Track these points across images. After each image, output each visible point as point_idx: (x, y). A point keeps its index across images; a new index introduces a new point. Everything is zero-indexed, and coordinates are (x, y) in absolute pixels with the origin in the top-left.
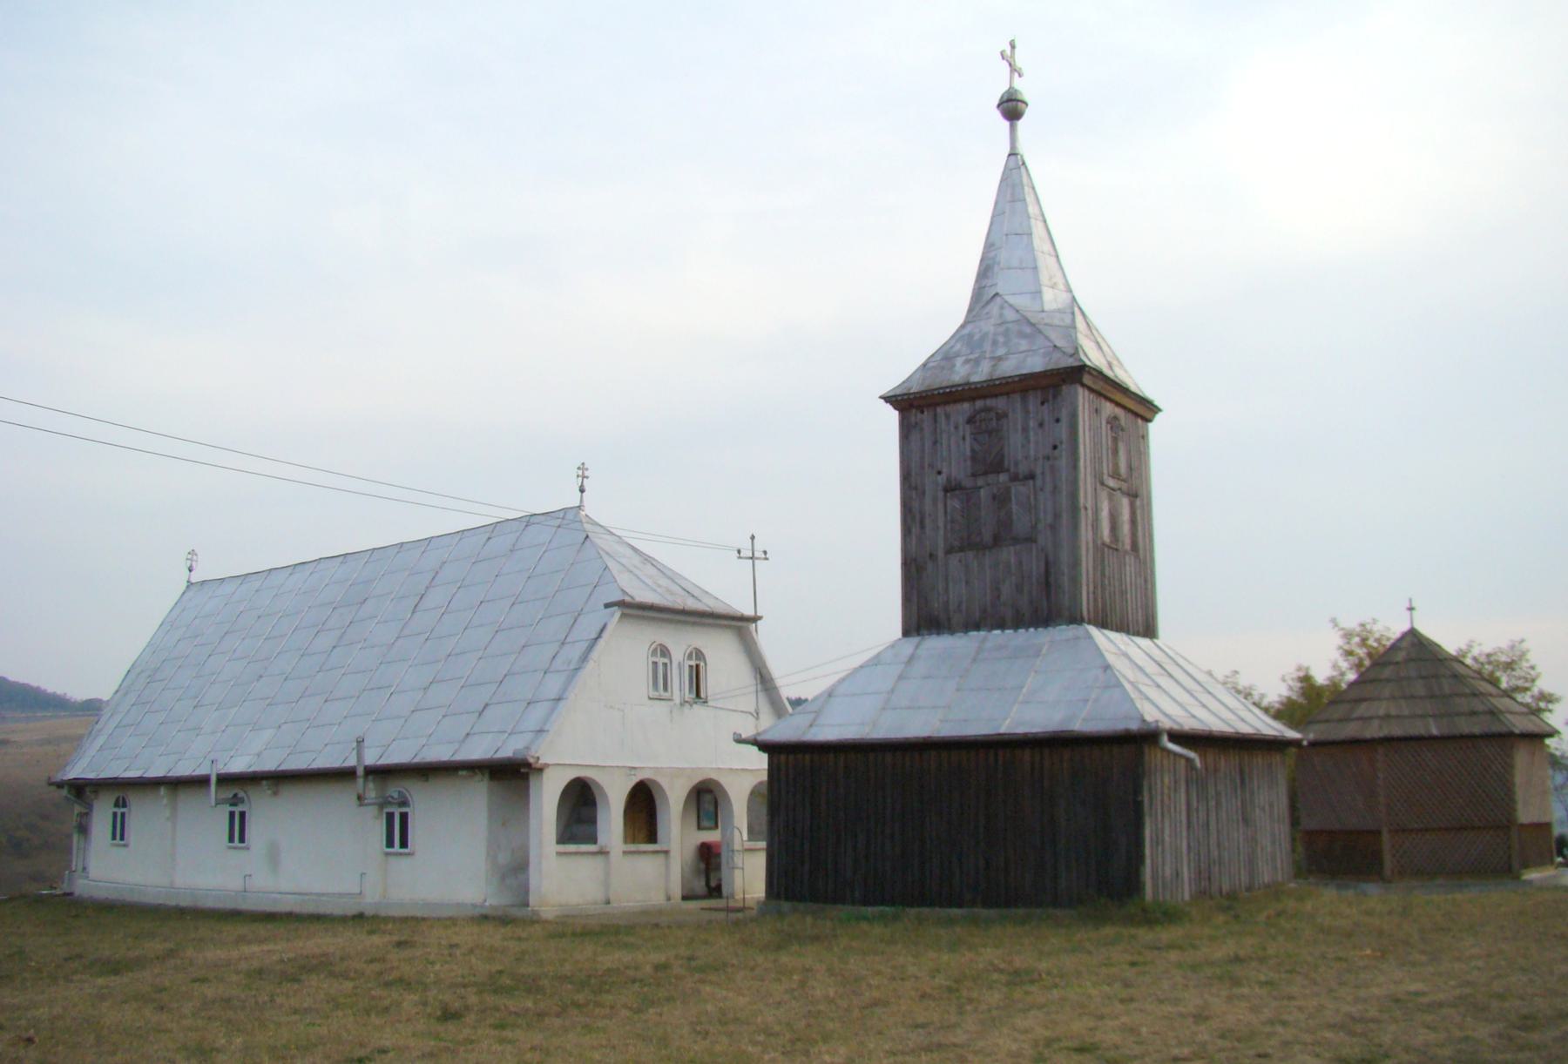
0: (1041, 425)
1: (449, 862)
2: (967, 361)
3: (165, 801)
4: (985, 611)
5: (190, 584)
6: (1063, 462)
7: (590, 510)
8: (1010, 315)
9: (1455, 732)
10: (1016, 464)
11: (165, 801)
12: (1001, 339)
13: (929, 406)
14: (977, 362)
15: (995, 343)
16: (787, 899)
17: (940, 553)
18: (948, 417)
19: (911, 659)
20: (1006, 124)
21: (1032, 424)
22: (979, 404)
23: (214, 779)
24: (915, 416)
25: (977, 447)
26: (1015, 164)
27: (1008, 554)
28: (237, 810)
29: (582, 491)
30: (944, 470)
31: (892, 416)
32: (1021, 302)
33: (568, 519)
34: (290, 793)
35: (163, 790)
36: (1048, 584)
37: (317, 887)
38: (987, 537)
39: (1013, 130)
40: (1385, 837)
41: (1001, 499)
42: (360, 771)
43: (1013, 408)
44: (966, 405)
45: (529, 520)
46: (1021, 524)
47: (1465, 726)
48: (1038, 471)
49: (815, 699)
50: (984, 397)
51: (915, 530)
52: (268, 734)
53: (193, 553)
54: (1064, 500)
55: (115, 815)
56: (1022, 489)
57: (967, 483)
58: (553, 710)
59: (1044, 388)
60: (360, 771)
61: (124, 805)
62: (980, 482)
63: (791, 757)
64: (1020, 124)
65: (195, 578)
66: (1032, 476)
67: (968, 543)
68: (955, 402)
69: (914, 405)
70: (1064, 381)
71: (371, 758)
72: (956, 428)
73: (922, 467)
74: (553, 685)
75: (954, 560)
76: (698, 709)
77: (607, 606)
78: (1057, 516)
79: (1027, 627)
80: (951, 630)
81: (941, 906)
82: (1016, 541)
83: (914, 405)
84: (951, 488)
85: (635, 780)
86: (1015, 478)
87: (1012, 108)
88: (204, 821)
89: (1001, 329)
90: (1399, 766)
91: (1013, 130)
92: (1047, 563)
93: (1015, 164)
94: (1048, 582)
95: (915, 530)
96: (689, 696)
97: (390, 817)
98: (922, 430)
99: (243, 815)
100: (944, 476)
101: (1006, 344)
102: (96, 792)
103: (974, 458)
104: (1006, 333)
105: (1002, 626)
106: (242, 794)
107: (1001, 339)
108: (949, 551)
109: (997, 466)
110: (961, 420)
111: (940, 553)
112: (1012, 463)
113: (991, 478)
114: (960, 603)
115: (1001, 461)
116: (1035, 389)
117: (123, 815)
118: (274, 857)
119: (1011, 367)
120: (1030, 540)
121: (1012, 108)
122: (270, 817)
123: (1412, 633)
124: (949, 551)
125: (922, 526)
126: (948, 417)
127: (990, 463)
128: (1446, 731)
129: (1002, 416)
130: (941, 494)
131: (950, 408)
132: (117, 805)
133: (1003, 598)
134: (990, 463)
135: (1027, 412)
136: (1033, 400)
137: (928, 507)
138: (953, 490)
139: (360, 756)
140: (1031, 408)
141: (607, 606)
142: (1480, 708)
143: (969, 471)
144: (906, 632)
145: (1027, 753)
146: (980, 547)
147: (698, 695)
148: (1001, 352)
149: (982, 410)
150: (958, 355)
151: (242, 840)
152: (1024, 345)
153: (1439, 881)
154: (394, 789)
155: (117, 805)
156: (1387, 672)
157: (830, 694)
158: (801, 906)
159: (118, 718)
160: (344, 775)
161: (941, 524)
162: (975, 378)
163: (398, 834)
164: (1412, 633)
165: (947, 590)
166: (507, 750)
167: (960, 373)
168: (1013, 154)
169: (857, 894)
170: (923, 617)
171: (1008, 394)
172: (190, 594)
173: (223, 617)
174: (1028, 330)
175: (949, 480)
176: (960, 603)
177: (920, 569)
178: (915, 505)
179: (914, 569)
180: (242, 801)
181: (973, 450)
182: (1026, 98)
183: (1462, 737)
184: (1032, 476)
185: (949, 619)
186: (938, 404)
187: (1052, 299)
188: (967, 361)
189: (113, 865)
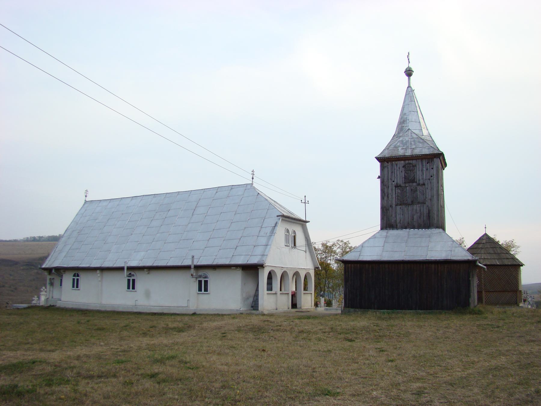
0: (427, 169)
1: (226, 296)
2: (402, 149)
3: (99, 275)
5: (86, 202)
6: (435, 181)
7: (254, 185)
8: (415, 136)
9: (492, 263)
10: (419, 180)
11: (99, 275)
12: (413, 143)
14: (406, 149)
15: (411, 144)
16: (351, 308)
17: (394, 206)
18: (397, 165)
19: (386, 237)
21: (424, 169)
22: (407, 162)
23: (126, 268)
24: (386, 164)
25: (406, 175)
27: (416, 207)
28: (131, 279)
29: (253, 179)
30: (395, 181)
31: (378, 164)
32: (417, 132)
33: (249, 187)
34: (154, 274)
35: (98, 272)
36: (429, 216)
37: (167, 304)
38: (409, 201)
39: (409, 80)
40: (483, 292)
41: (414, 191)
42: (192, 267)
43: (419, 164)
44: (403, 162)
45: (232, 187)
46: (421, 198)
47: (506, 262)
49: (359, 246)
50: (409, 160)
51: (386, 198)
52: (142, 254)
53: (87, 191)
54: (435, 192)
55: (74, 279)
56: (421, 188)
57: (403, 185)
58: (266, 248)
60: (192, 267)
61: (78, 276)
62: (407, 185)
63: (353, 265)
64: (411, 77)
65: (88, 199)
66: (424, 184)
67: (402, 203)
68: (399, 160)
69: (384, 161)
70: (435, 157)
71: (196, 263)
72: (399, 168)
74: (263, 241)
75: (398, 207)
76: (294, 250)
77: (277, 216)
78: (432, 196)
79: (422, 228)
82: (419, 203)
84: (397, 186)
85: (283, 271)
86: (419, 185)
87: (409, 73)
88: (122, 279)
89: (413, 140)
90: (489, 272)
91: (409, 80)
93: (410, 92)
94: (429, 215)
95: (386, 198)
96: (293, 245)
97: (200, 282)
98: (388, 168)
99: (134, 280)
100: (395, 182)
101: (415, 144)
102: (64, 271)
103: (405, 177)
104: (414, 141)
105: (414, 228)
106: (133, 273)
107: (413, 143)
109: (413, 181)
110: (401, 166)
111: (394, 206)
112: (411, 180)
114: (400, 220)
115: (414, 179)
116: (425, 159)
117: (78, 280)
118: (148, 294)
119: (417, 152)
120: (424, 203)
121: (409, 73)
122: (143, 281)
123: (486, 234)
125: (388, 197)
126: (397, 165)
127: (410, 179)
128: (501, 264)
129: (414, 166)
130: (394, 188)
132: (74, 276)
133: (415, 220)
134: (410, 179)
135: (423, 165)
136: (424, 162)
137: (390, 191)
139: (193, 261)
140: (424, 164)
141: (277, 216)
142: (509, 257)
144: (382, 229)
145: (367, 265)
146: (407, 204)
147: (295, 245)
148: (414, 147)
150: (399, 147)
151: (77, 287)
152: (421, 145)
153: (498, 306)
154: (201, 272)
155: (74, 276)
156: (480, 246)
157: (362, 246)
158: (357, 310)
159: (68, 247)
160: (188, 267)
161: (394, 196)
162: (406, 154)
163: (203, 286)
164: (486, 234)
165: (396, 216)
166: (254, 260)
167: (401, 152)
168: (409, 87)
170: (388, 223)
172: (86, 205)
173: (97, 214)
174: (421, 141)
175: (397, 184)
176: (400, 220)
177: (387, 210)
178: (386, 190)
179: (385, 210)
180: (133, 275)
182: (413, 70)
183: (506, 265)
184: (424, 184)
185: (397, 225)
187: (425, 132)
188: (402, 149)
189: (67, 295)
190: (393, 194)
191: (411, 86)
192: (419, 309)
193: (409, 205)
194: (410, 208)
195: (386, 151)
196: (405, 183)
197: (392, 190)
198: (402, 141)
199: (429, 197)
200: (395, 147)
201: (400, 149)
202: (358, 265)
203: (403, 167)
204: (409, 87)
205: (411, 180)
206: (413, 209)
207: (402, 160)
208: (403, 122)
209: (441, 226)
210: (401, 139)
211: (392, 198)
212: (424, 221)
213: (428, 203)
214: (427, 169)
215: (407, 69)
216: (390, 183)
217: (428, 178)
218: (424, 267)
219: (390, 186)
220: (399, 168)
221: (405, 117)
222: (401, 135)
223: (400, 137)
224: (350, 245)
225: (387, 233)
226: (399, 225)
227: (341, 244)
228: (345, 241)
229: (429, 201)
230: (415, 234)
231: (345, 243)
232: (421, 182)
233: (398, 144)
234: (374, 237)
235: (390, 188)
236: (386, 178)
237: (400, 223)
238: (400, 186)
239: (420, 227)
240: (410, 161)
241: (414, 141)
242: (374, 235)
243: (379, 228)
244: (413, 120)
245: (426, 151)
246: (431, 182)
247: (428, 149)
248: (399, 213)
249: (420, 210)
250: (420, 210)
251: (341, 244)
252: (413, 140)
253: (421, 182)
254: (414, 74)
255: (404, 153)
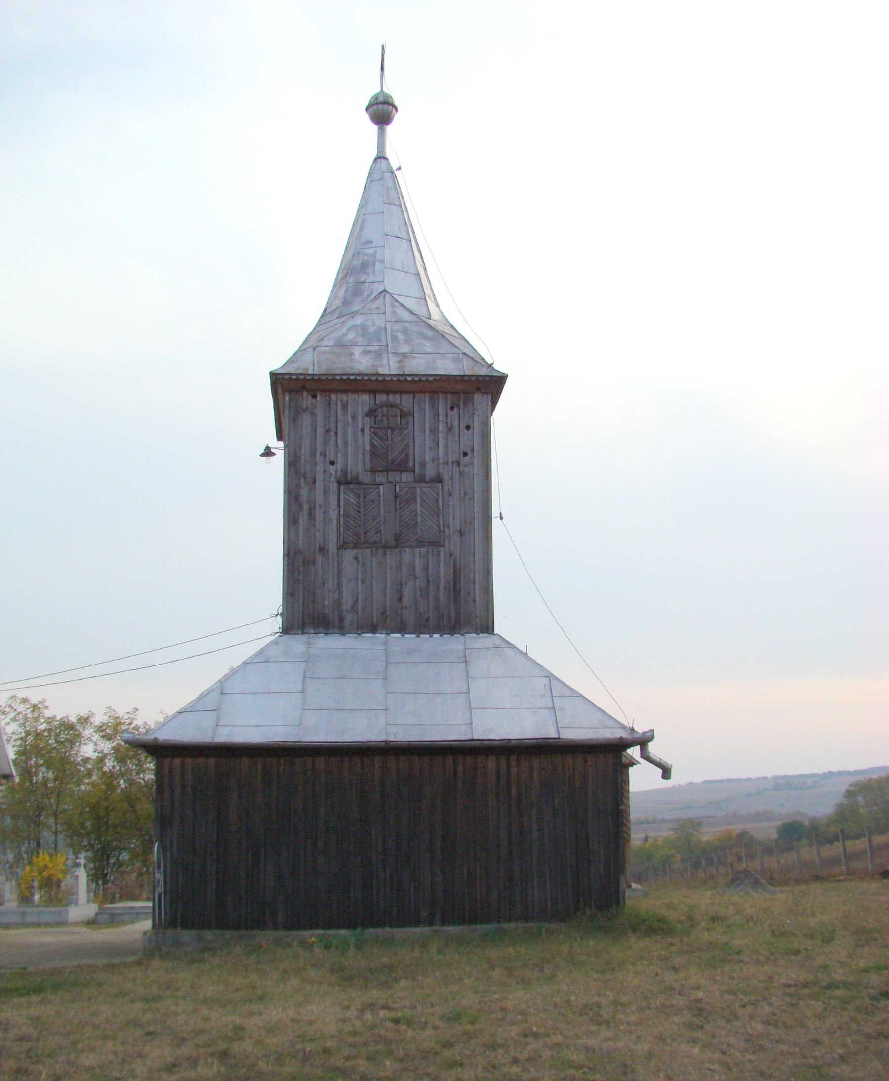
4: (384, 613)
8: (406, 316)
10: (423, 465)
12: (401, 337)
13: (323, 391)
14: (378, 355)
15: (394, 339)
16: (185, 926)
17: (332, 548)
18: (345, 406)
19: (307, 659)
20: (375, 128)
22: (382, 398)
26: (382, 177)
36: (456, 591)
38: (388, 535)
41: (401, 500)
43: (423, 411)
44: (366, 397)
48: (446, 477)
50: (388, 392)
51: (303, 520)
56: (427, 490)
57: (365, 478)
59: (455, 393)
62: (380, 478)
64: (390, 129)
67: (357, 539)
70: (478, 389)
72: (354, 418)
73: (313, 455)
75: (348, 555)
79: (431, 632)
80: (342, 630)
81: (391, 926)
82: (421, 543)
83: (289, 388)
84: (345, 481)
86: (421, 479)
87: (382, 112)
92: (455, 571)
93: (382, 177)
95: (303, 520)
98: (313, 415)
100: (339, 466)
101: (407, 342)
103: (374, 452)
104: (405, 331)
105: (402, 629)
107: (401, 337)
108: (342, 546)
109: (402, 466)
111: (332, 548)
112: (385, 457)
113: (393, 476)
116: (445, 393)
119: (418, 365)
120: (438, 544)
121: (382, 112)
124: (342, 546)
125: (311, 516)
127: (389, 461)
130: (334, 487)
131: (351, 397)
133: (406, 601)
134: (389, 461)
135: (437, 415)
137: (319, 498)
138: (348, 483)
143: (368, 466)
144: (286, 630)
145: (245, 760)
148: (404, 349)
149: (382, 405)
150: (353, 344)
152: (428, 347)
161: (334, 515)
162: (382, 371)
165: (339, 586)
167: (361, 362)
168: (381, 157)
169: (280, 917)
170: (309, 609)
171: (414, 393)
174: (430, 333)
175: (344, 472)
177: (309, 562)
178: (304, 492)
179: (298, 563)
181: (373, 445)
184: (439, 480)
185: (341, 619)
186: (332, 391)
188: (366, 353)
190: (331, 507)
191: (389, 153)
192: (444, 922)
193: (385, 547)
194: (391, 558)
195: (308, 357)
196: (373, 471)
197: (326, 492)
198: (364, 328)
199: (455, 524)
200: (340, 344)
201: (357, 351)
202: (212, 761)
203: (368, 415)
204: (381, 157)
205: (385, 457)
206: (399, 565)
207: (364, 391)
208: (358, 275)
209: (486, 627)
210: (358, 320)
211: (327, 522)
212: (437, 607)
213: (453, 544)
214: (450, 430)
215: (376, 97)
216: (319, 469)
217: (453, 457)
218: (460, 768)
219: (320, 478)
220: (354, 418)
221: (370, 251)
222: (356, 307)
223: (354, 314)
224: (48, 714)
225: (308, 644)
226: (348, 618)
227: (21, 708)
228: (34, 701)
229: (456, 538)
230: (411, 652)
231: (35, 707)
232: (430, 471)
233: (351, 336)
234: (261, 658)
235: (319, 485)
236: (305, 451)
237: (353, 609)
238: (356, 481)
239: (423, 626)
240: (391, 397)
241: (405, 331)
242: (261, 651)
243: (277, 624)
244: (397, 265)
245: (447, 367)
246: (461, 473)
247: (456, 360)
248: (351, 578)
249: (426, 568)
250: (426, 568)
251: (21, 708)
252: (399, 327)
253: (430, 471)
254: (397, 119)
255: (375, 366)
